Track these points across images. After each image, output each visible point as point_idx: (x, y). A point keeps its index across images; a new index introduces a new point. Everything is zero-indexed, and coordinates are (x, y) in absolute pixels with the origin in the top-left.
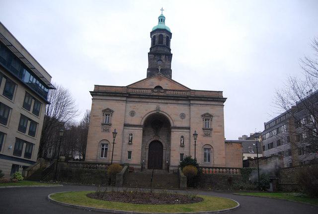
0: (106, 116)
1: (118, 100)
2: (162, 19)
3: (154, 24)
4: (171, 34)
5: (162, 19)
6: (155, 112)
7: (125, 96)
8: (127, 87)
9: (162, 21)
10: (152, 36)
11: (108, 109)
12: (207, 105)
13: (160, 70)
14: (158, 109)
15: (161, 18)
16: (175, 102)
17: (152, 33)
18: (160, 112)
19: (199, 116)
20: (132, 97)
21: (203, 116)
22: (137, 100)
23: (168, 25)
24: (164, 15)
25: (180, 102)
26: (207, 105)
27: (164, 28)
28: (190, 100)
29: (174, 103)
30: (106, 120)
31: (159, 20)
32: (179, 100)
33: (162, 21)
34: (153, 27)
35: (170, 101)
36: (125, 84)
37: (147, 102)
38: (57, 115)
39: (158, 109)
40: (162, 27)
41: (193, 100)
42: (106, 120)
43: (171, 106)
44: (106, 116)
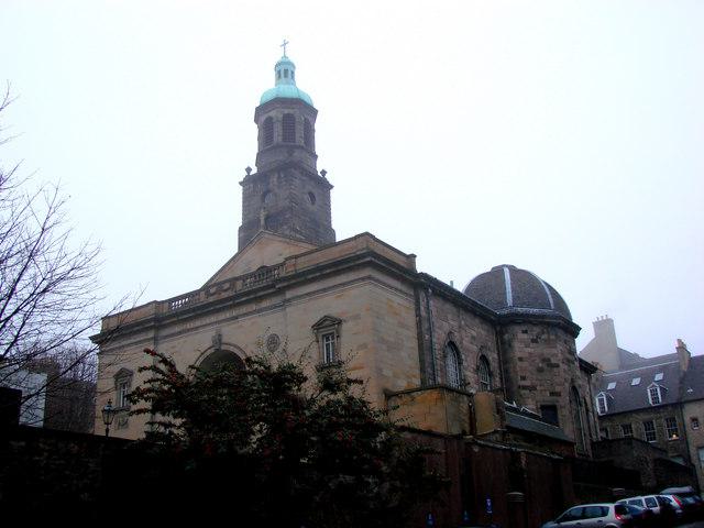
0: (328, 339)
1: (314, 293)
2: (285, 71)
3: (265, 85)
4: (314, 112)
5: (285, 71)
6: (212, 350)
7: (151, 328)
8: (206, 288)
9: (286, 76)
10: (263, 118)
11: (325, 318)
12: (324, 290)
13: (262, 222)
14: (218, 340)
15: (282, 68)
16: (254, 307)
17: (260, 111)
18: (224, 347)
19: (308, 331)
20: (165, 326)
21: (318, 326)
22: (177, 329)
23: (306, 84)
24: (292, 59)
25: (265, 304)
26: (324, 290)
27: (295, 95)
28: (281, 291)
29: (251, 313)
30: (328, 354)
31: (279, 72)
32: (261, 299)
33: (286, 76)
34: (261, 94)
35: (244, 310)
36: (196, 283)
37: (197, 328)
38: (351, 365)
39: (218, 340)
40: (287, 91)
41: (289, 287)
42: (328, 354)
43: (246, 322)
44: (328, 339)
